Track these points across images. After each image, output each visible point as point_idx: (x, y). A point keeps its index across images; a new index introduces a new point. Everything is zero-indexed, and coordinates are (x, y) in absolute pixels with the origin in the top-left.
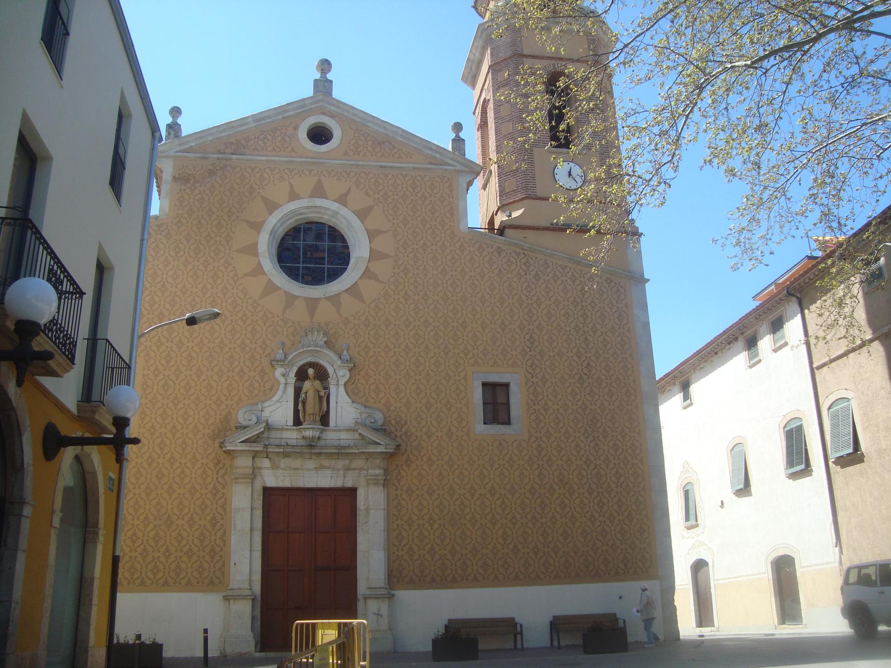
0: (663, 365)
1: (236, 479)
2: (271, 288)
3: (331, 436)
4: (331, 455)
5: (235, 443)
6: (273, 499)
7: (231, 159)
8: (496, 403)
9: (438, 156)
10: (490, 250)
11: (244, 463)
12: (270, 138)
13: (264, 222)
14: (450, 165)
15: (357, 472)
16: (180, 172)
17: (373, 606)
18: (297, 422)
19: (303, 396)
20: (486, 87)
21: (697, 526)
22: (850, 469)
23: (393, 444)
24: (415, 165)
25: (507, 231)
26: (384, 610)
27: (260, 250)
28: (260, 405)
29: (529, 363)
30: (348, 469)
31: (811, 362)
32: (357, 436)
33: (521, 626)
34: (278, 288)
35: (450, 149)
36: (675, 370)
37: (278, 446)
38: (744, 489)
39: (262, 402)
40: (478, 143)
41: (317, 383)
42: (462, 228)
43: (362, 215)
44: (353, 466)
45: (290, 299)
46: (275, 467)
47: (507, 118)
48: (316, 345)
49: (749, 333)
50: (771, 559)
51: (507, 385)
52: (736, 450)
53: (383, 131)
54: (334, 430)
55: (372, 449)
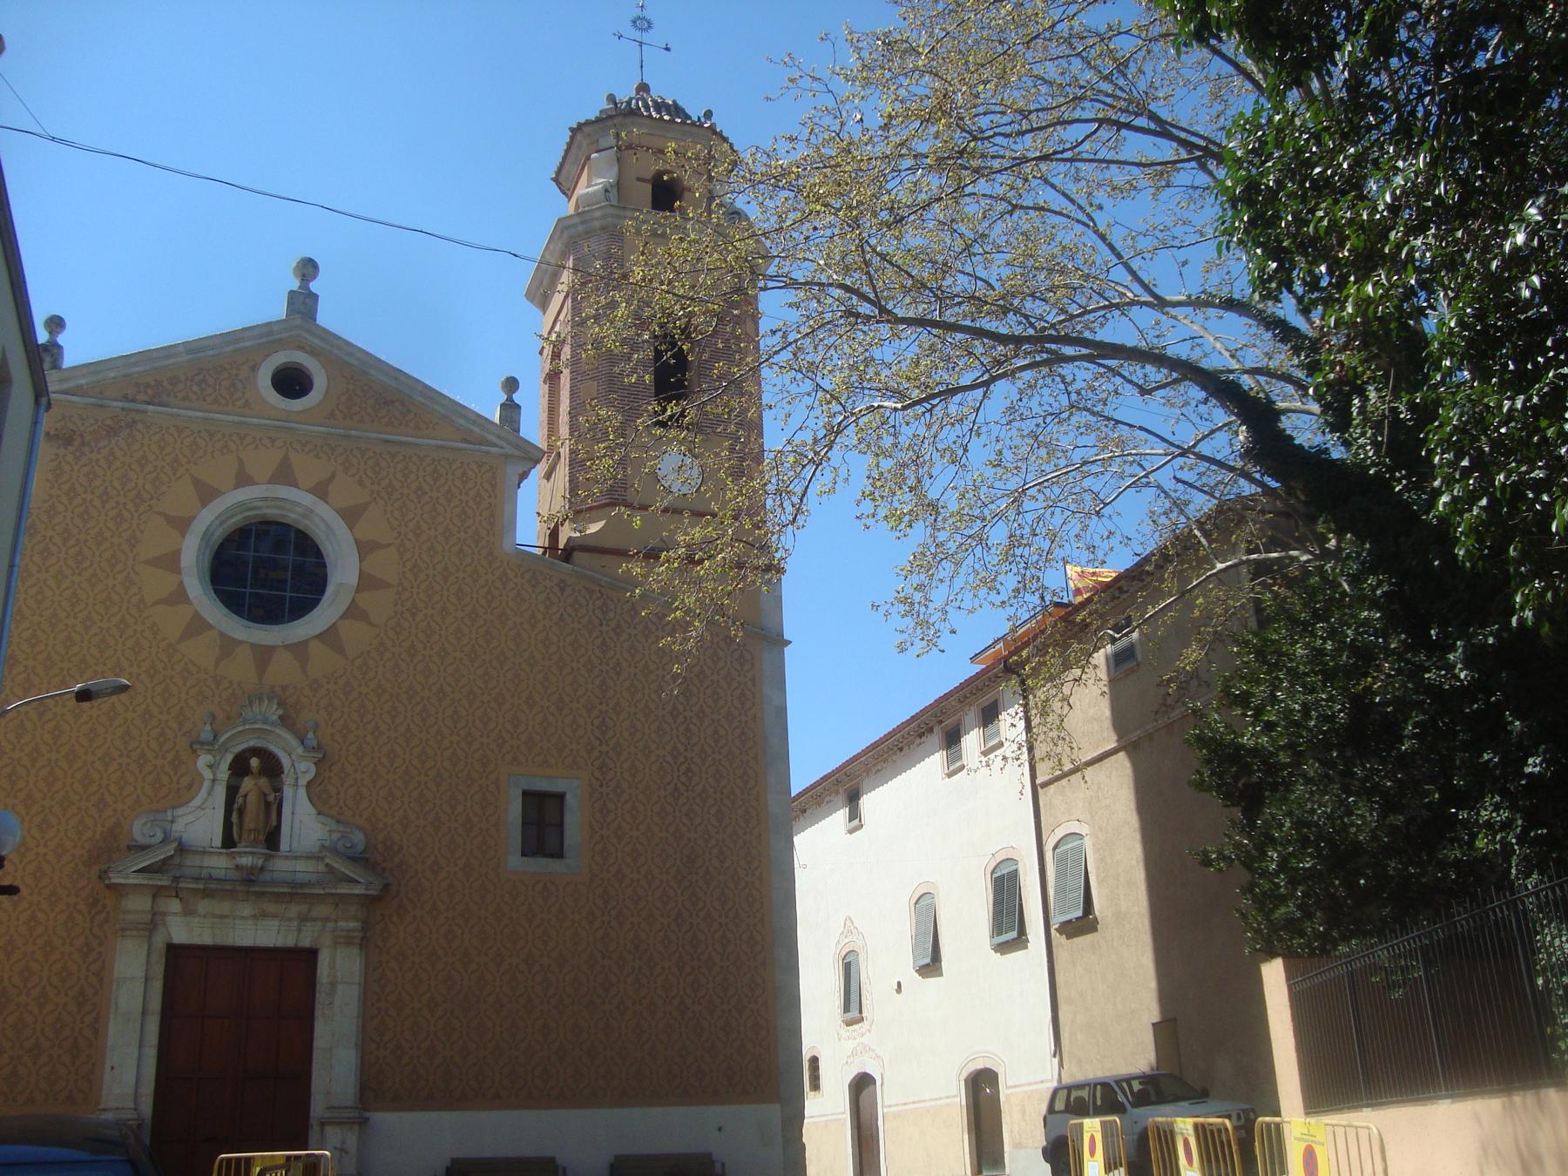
0: (803, 772)
1: (123, 930)
2: (198, 625)
3: (281, 866)
4: (278, 897)
5: (126, 873)
6: (182, 963)
7: (145, 412)
8: (543, 820)
9: (476, 429)
10: (548, 584)
11: (138, 905)
12: (211, 381)
13: (193, 518)
14: (495, 445)
15: (319, 923)
16: (58, 426)
17: (333, 1134)
18: (229, 841)
19: (240, 800)
20: (561, 317)
21: (862, 1020)
22: (1079, 941)
23: (377, 883)
24: (440, 443)
25: (577, 555)
26: (352, 1140)
27: (183, 564)
28: (169, 813)
29: (597, 764)
30: (306, 920)
31: (1033, 777)
32: (321, 868)
33: (564, 1169)
34: (211, 627)
35: (497, 421)
36: (838, 770)
37: (197, 879)
38: (931, 965)
39: (174, 808)
40: (544, 403)
41: (263, 781)
42: (507, 546)
43: (351, 516)
44: (314, 914)
45: (228, 645)
46: (188, 912)
47: (586, 371)
48: (265, 721)
49: (950, 722)
50: (965, 1074)
51: (561, 797)
52: (923, 902)
53: (393, 383)
54: (287, 858)
55: (344, 889)
